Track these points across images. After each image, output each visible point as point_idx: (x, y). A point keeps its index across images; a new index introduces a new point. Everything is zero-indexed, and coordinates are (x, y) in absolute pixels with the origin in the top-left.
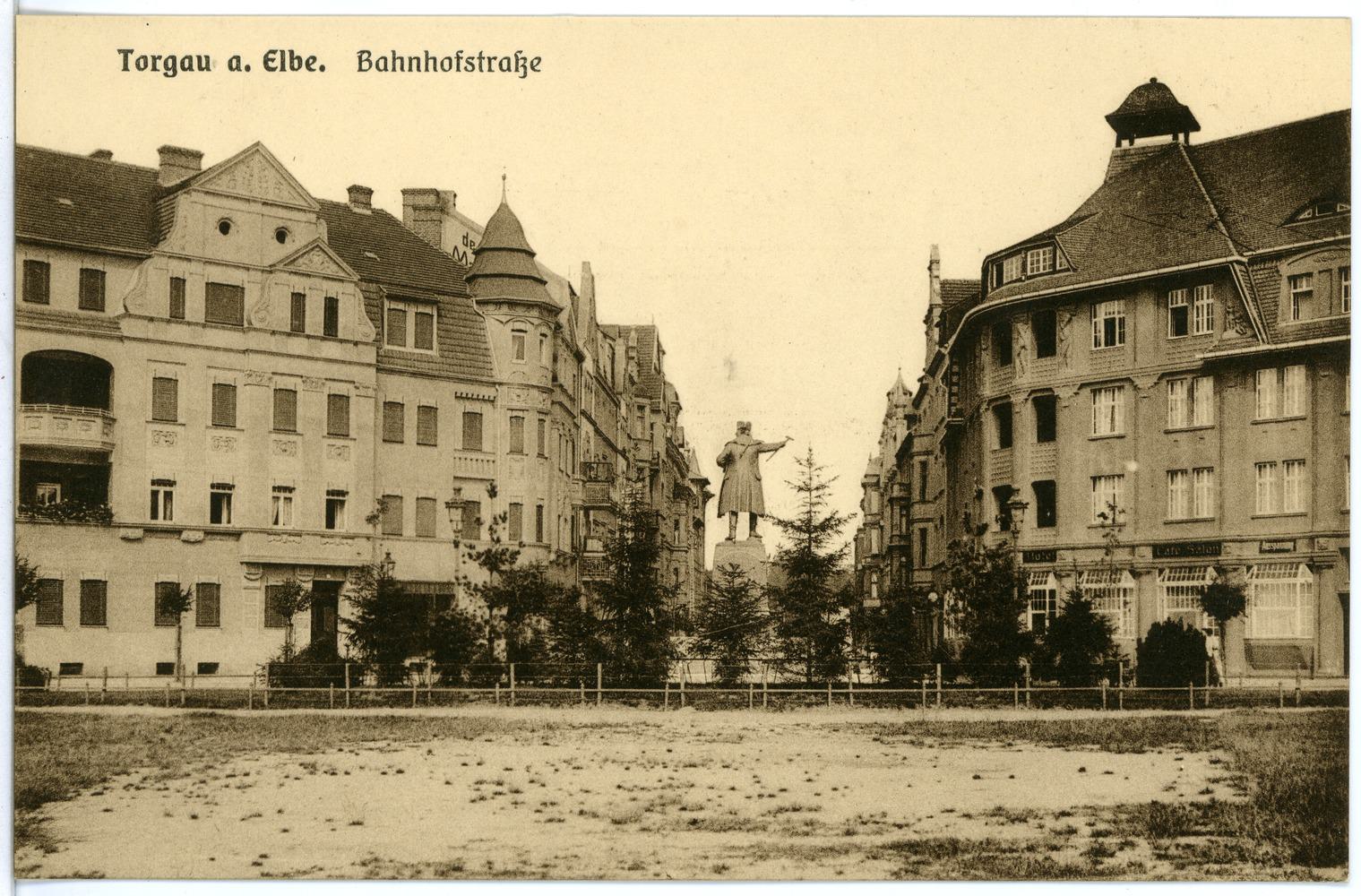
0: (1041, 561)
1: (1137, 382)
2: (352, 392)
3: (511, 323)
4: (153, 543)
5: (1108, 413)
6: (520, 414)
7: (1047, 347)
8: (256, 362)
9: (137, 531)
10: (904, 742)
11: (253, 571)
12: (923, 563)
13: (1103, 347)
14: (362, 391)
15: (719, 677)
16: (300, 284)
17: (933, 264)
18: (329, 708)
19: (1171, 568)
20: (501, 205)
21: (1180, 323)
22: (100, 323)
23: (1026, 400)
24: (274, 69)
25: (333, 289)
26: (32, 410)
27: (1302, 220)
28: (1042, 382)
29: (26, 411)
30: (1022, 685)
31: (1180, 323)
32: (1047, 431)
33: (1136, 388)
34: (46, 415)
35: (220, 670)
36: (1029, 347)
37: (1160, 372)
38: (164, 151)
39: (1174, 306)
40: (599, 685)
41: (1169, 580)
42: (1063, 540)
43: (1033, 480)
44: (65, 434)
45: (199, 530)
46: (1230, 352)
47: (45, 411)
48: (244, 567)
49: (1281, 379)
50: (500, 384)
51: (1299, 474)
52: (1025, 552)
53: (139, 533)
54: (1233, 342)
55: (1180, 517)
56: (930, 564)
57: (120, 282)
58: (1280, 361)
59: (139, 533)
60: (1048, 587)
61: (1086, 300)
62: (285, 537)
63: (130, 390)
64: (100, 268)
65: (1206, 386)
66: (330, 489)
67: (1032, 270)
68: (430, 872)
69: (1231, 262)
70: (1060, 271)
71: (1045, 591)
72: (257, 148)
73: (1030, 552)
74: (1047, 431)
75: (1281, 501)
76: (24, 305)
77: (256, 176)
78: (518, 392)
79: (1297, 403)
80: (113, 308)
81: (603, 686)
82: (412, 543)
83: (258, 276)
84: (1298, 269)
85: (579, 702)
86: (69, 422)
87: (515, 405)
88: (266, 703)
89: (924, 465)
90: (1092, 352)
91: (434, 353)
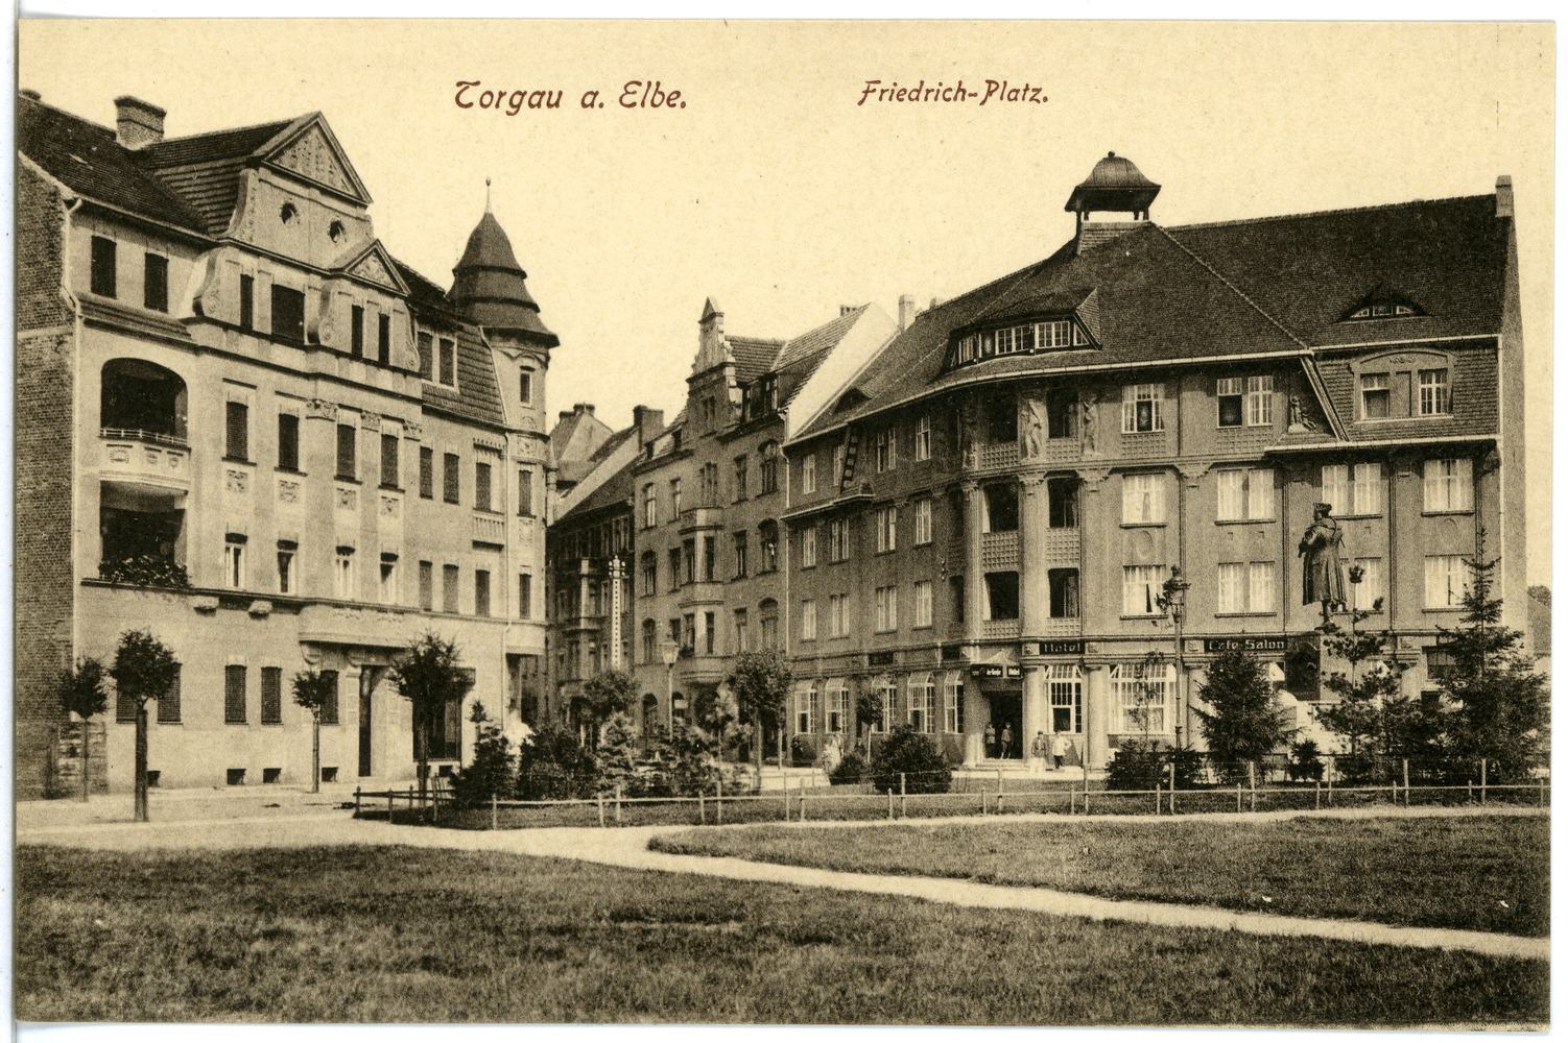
0: (1063, 653)
1: (1182, 470)
2: (401, 434)
3: (520, 359)
4: (225, 616)
5: (1144, 499)
6: (528, 468)
7: (1060, 427)
8: (325, 390)
9: (209, 598)
10: (502, 871)
11: (315, 652)
12: (710, 650)
13: (1136, 431)
14: (410, 433)
15: (1340, 773)
16: (361, 296)
17: (709, 318)
18: (1236, 811)
19: (1055, 666)
20: (485, 215)
21: (1231, 410)
22: (162, 324)
23: (1041, 481)
25: (387, 304)
26: (119, 438)
27: (1356, 319)
28: (1064, 463)
29: (109, 437)
30: (1401, 783)
31: (1231, 410)
32: (1063, 513)
33: (1180, 476)
34: (136, 445)
35: (281, 777)
36: (1043, 426)
37: (1211, 463)
38: (124, 103)
39: (1224, 394)
40: (1484, 782)
41: (1054, 676)
42: (1091, 631)
43: (1050, 567)
44: (156, 470)
45: (213, 595)
46: (1305, 447)
47: (135, 438)
48: (306, 650)
49: (1351, 477)
50: (511, 431)
52: (1042, 644)
53: (213, 602)
54: (1302, 438)
55: (1231, 610)
56: (718, 650)
57: (187, 277)
58: (1349, 459)
59: (213, 602)
60: (1074, 680)
61: (1107, 386)
62: (348, 611)
63: (202, 415)
64: (163, 254)
65: (1264, 480)
66: (341, 544)
67: (1041, 343)
68: (70, 1015)
69: (1303, 356)
70: (1078, 348)
71: (1070, 685)
72: (315, 122)
73: (1049, 643)
74: (1063, 513)
75: (1247, 598)
76: (93, 296)
77: (314, 154)
78: (528, 441)
79: (1461, 499)
80: (180, 307)
81: (1411, 784)
82: (472, 623)
83: (316, 280)
84: (1371, 368)
85: (1467, 799)
86: (179, 458)
87: (525, 456)
88: (1172, 807)
89: (709, 541)
90: (1124, 436)
91: (455, 389)
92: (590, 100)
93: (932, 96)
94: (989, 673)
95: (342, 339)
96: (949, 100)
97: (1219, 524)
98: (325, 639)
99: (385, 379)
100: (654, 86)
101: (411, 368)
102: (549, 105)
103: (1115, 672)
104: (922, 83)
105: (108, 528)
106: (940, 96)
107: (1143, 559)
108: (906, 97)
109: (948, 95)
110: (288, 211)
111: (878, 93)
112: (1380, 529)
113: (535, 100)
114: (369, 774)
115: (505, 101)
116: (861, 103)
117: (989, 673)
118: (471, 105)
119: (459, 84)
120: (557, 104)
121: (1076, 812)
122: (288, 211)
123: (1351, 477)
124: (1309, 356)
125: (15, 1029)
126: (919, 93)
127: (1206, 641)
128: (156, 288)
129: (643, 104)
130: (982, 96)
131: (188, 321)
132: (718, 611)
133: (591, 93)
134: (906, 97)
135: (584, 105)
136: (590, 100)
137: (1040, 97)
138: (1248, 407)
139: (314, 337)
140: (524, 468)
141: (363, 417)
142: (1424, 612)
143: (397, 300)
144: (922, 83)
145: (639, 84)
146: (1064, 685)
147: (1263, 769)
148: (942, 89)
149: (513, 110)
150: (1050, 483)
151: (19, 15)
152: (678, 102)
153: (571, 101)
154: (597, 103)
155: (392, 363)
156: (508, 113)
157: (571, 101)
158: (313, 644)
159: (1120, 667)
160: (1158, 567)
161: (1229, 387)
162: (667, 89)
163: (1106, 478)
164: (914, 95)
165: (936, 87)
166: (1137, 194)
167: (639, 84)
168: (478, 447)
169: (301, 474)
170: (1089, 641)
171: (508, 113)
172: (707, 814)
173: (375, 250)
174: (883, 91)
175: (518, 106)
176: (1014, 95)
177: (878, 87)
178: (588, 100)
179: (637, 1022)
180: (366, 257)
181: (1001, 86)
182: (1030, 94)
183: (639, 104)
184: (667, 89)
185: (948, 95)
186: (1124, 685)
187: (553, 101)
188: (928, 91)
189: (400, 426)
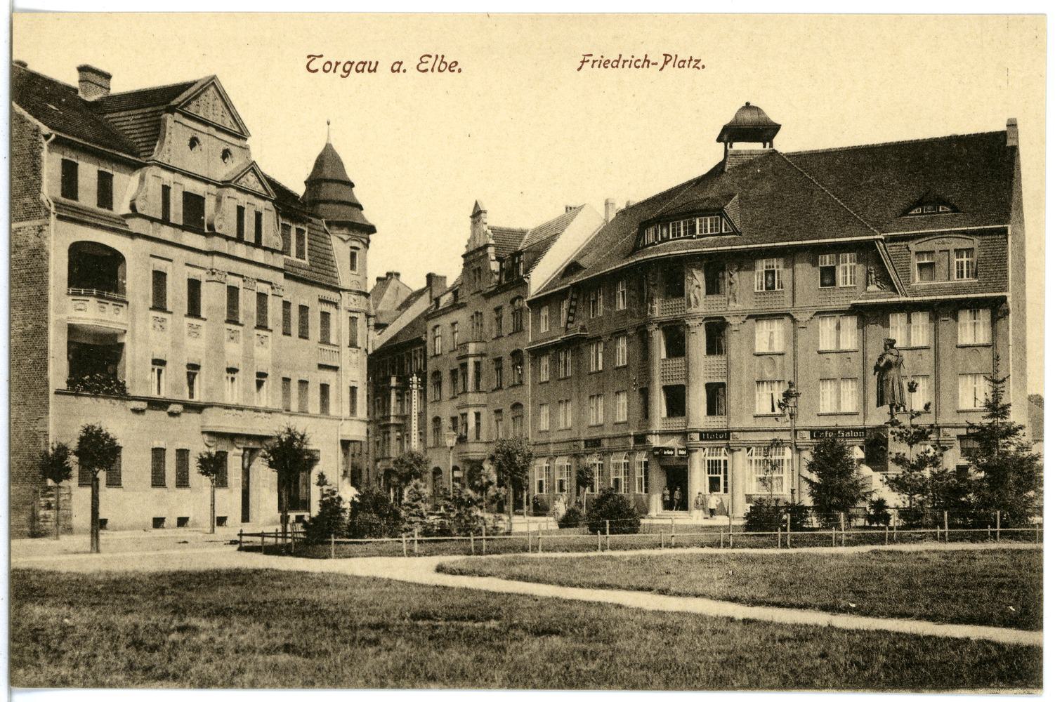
0: (715, 439)
1: (795, 316)
2: (270, 292)
3: (350, 242)
4: (151, 415)
5: (769, 336)
6: (355, 315)
7: (713, 287)
8: (219, 262)
9: (141, 403)
10: (338, 586)
11: (212, 439)
12: (478, 438)
13: (764, 290)
14: (276, 292)
15: (902, 521)
16: (243, 199)
17: (477, 214)
18: (832, 546)
19: (710, 448)
20: (327, 145)
21: (828, 276)
22: (109, 218)
23: (701, 324)
24: (638, 67)
25: (260, 204)
26: (80, 294)
27: (913, 215)
28: (716, 312)
29: (73, 294)
30: (942, 527)
31: (828, 276)
32: (715, 345)
33: (794, 321)
34: (92, 299)
35: (189, 523)
36: (701, 286)
37: (815, 312)
38: (83, 69)
39: (823, 265)
40: (998, 526)
41: (709, 455)
42: (734, 424)
43: (706, 382)
44: (105, 316)
45: (144, 400)
46: (878, 301)
47: (91, 295)
48: (206, 438)
49: (909, 321)
50: (344, 290)
51: (831, 387)
52: (701, 434)
53: (143, 405)
54: (876, 295)
55: (828, 410)
56: (483, 437)
57: (126, 186)
58: (908, 309)
59: (143, 405)
60: (722, 458)
61: (745, 260)
62: (234, 411)
63: (136, 279)
64: (110, 171)
65: (850, 323)
66: (229, 366)
67: (701, 231)
69: (877, 240)
70: (725, 234)
71: (720, 461)
72: (212, 82)
73: (705, 433)
74: (715, 345)
75: (839, 402)
76: (63, 200)
77: (211, 104)
78: (356, 297)
79: (983, 336)
80: (121, 207)
81: (949, 528)
82: (318, 420)
83: (213, 189)
84: (922, 247)
85: (987, 538)
86: (121, 308)
87: (353, 307)
88: (788, 543)
89: (477, 364)
90: (756, 293)
91: (306, 262)
92: (397, 67)
93: (627, 64)
94: (665, 453)
95: (230, 228)
96: (638, 67)
97: (820, 353)
98: (219, 430)
99: (259, 255)
100: (440, 58)
101: (276, 248)
102: (369, 71)
103: (750, 452)
104: (620, 56)
105: (73, 355)
106: (633, 65)
107: (769, 376)
108: (609, 65)
109: (638, 64)
110: (194, 142)
111: (591, 63)
112: (928, 356)
113: (360, 67)
114: (248, 521)
115: (340, 68)
116: (579, 69)
117: (665, 453)
118: (317, 70)
119: (309, 57)
120: (375, 70)
121: (724, 547)
122: (194, 142)
123: (909, 321)
124: (881, 240)
125: (10, 692)
126: (618, 63)
127: (812, 431)
129: (432, 70)
130: (661, 65)
131: (126, 216)
132: (483, 411)
133: (398, 62)
134: (609, 65)
135: (393, 71)
136: (397, 67)
137: (700, 65)
138: (840, 274)
139: (211, 227)
140: (353, 315)
141: (244, 281)
142: (958, 412)
143: (267, 202)
144: (620, 56)
145: (430, 56)
146: (716, 461)
147: (850, 518)
148: (634, 60)
149: (345, 74)
150: (706, 325)
151: (13, 10)
152: (456, 69)
153: (384, 68)
154: (401, 70)
156: (342, 76)
157: (384, 68)
158: (211, 434)
159: (754, 449)
160: (779, 382)
161: (827, 260)
162: (449, 60)
163: (744, 322)
164: (615, 64)
165: (630, 58)
166: (765, 131)
167: (430, 56)
168: (322, 301)
169: (202, 319)
170: (732, 431)
171: (342, 76)
172: (476, 548)
173: (253, 168)
174: (594, 61)
175: (349, 72)
176: (682, 64)
177: (591, 59)
178: (396, 67)
179: (428, 688)
180: (246, 173)
181: (674, 58)
182: (693, 63)
183: (430, 70)
184: (449, 60)
185: (638, 64)
186: (756, 461)
187: (372, 68)
188: (625, 61)
189: (269, 287)
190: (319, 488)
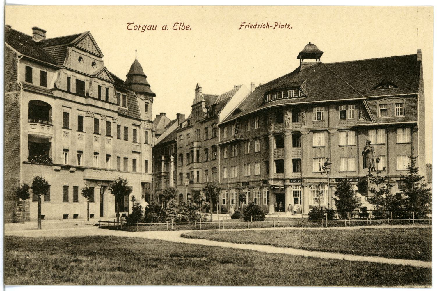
0: (296, 182)
1: (330, 131)
2: (112, 121)
3: (145, 100)
4: (63, 172)
5: (319, 139)
6: (147, 131)
7: (295, 119)
8: (91, 109)
9: (58, 167)
11: (88, 182)
12: (198, 181)
13: (316, 120)
14: (114, 121)
15: (373, 216)
16: (101, 83)
17: (198, 89)
18: (345, 226)
19: (294, 186)
20: (135, 60)
21: (343, 115)
22: (45, 91)
23: (290, 134)
24: (264, 28)
25: (108, 85)
26: (33, 122)
27: (378, 89)
28: (296, 129)
29: (30, 122)
30: (390, 219)
31: (343, 115)
32: (296, 143)
33: (329, 133)
34: (38, 124)
35: (78, 217)
36: (291, 119)
37: (338, 129)
38: (35, 29)
39: (341, 110)
40: (414, 218)
41: (294, 189)
42: (304, 176)
43: (293, 158)
44: (44, 131)
45: (59, 166)
46: (364, 125)
47: (38, 122)
48: (85, 181)
49: (377, 133)
50: (142, 120)
51: (344, 160)
52: (290, 180)
53: (59, 168)
54: (363, 122)
55: (343, 170)
56: (200, 181)
57: (52, 77)
58: (376, 128)
59: (59, 168)
60: (299, 190)
61: (308, 108)
62: (97, 170)
63: (56, 116)
64: (45, 71)
65: (352, 134)
66: (95, 152)
67: (290, 96)
69: (363, 99)
70: (300, 97)
71: (298, 191)
72: (88, 34)
73: (292, 179)
74: (296, 143)
75: (347, 167)
76: (26, 83)
77: (87, 43)
78: (147, 123)
79: (407, 139)
80: (50, 86)
81: (393, 219)
82: (132, 174)
83: (88, 78)
84: (382, 103)
85: (409, 223)
86: (50, 128)
87: (146, 127)
88: (327, 225)
89: (198, 151)
90: (313, 122)
91: (127, 109)
92: (164, 28)
93: (260, 27)
95: (95, 95)
96: (264, 28)
97: (340, 146)
98: (91, 178)
99: (107, 106)
100: (182, 24)
101: (115, 103)
102: (153, 29)
103: (311, 187)
104: (257, 23)
106: (262, 27)
107: (319, 156)
108: (252, 27)
109: (264, 26)
110: (80, 59)
111: (245, 26)
112: (385, 148)
113: (149, 28)
115: (141, 28)
116: (240, 29)
118: (131, 29)
119: (128, 23)
120: (155, 29)
121: (300, 227)
122: (80, 59)
123: (377, 133)
124: (365, 99)
125: (4, 287)
126: (256, 26)
127: (336, 179)
128: (44, 80)
129: (179, 29)
130: (274, 27)
131: (52, 90)
132: (200, 170)
133: (165, 26)
134: (252, 27)
135: (163, 29)
136: (164, 28)
137: (290, 27)
138: (348, 114)
139: (87, 94)
140: (146, 130)
141: (101, 116)
142: (397, 171)
143: (111, 84)
144: (257, 23)
145: (178, 23)
146: (297, 191)
148: (263, 25)
149: (143, 31)
150: (293, 135)
151: (5, 4)
152: (189, 28)
153: (159, 28)
154: (166, 29)
155: (109, 101)
156: (142, 32)
157: (159, 28)
158: (87, 180)
159: (312, 186)
160: (323, 158)
161: (343, 108)
162: (186, 25)
163: (308, 133)
164: (255, 26)
165: (261, 24)
166: (317, 54)
167: (178, 23)
168: (133, 125)
170: (303, 179)
171: (142, 32)
173: (105, 70)
174: (246, 25)
175: (144, 30)
176: (282, 27)
177: (245, 24)
178: (164, 28)
179: (177, 285)
180: (102, 72)
181: (279, 24)
182: (287, 26)
183: (178, 29)
184: (186, 25)
185: (264, 26)
186: (313, 191)
187: (154, 28)
188: (259, 25)
189: (111, 119)
190: (132, 202)
